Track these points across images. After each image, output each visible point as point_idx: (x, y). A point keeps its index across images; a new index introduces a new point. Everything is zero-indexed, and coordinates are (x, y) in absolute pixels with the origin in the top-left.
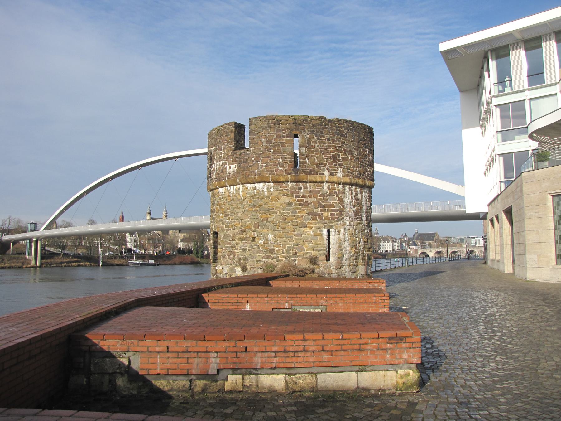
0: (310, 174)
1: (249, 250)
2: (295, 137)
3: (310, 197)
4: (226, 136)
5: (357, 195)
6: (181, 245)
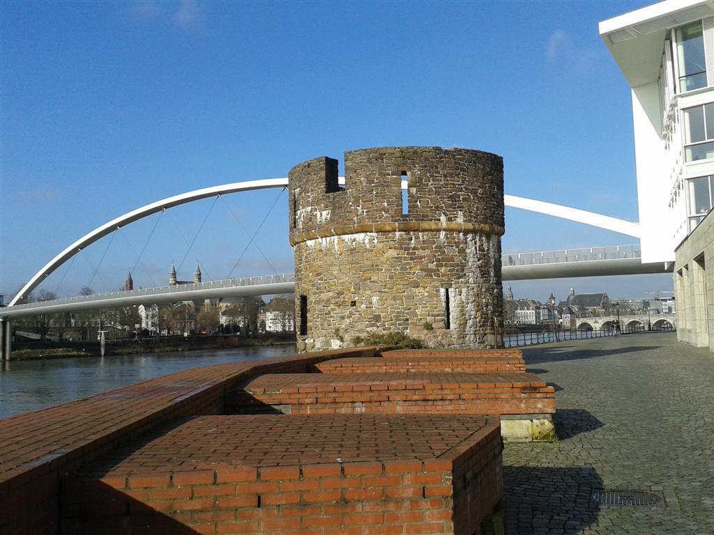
0: (423, 220)
1: (349, 317)
2: (402, 175)
3: (423, 249)
6: (223, 320)
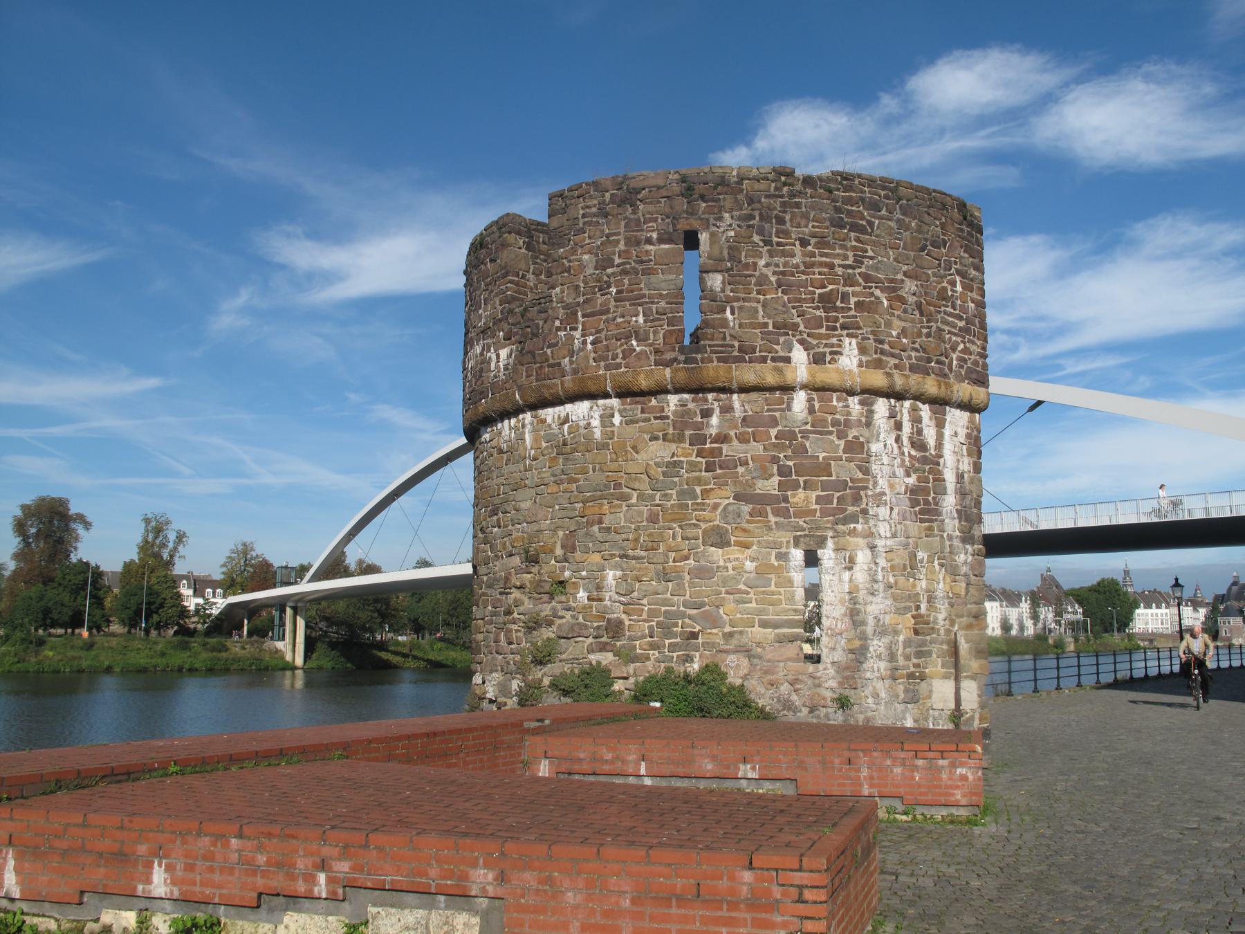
0: (739, 360)
3: (743, 439)
4: (491, 261)
5: (920, 432)
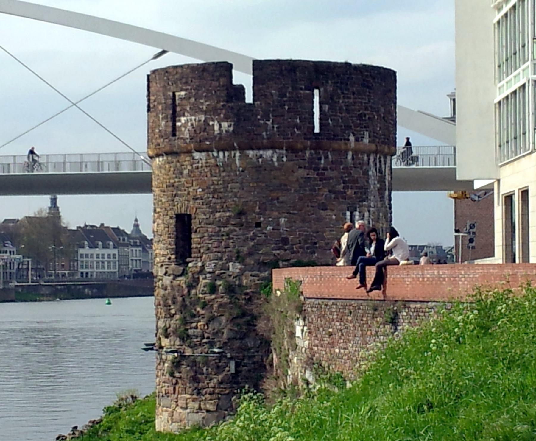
0: (333, 139)
